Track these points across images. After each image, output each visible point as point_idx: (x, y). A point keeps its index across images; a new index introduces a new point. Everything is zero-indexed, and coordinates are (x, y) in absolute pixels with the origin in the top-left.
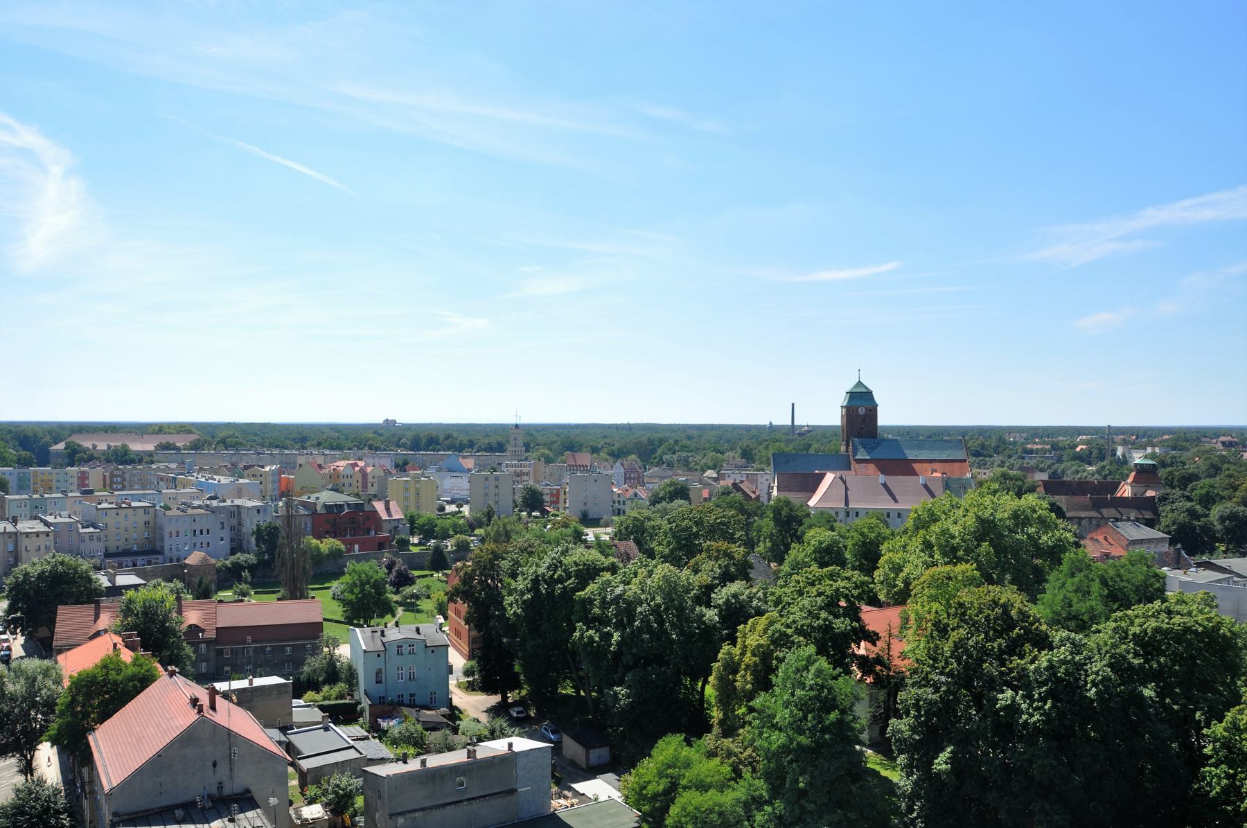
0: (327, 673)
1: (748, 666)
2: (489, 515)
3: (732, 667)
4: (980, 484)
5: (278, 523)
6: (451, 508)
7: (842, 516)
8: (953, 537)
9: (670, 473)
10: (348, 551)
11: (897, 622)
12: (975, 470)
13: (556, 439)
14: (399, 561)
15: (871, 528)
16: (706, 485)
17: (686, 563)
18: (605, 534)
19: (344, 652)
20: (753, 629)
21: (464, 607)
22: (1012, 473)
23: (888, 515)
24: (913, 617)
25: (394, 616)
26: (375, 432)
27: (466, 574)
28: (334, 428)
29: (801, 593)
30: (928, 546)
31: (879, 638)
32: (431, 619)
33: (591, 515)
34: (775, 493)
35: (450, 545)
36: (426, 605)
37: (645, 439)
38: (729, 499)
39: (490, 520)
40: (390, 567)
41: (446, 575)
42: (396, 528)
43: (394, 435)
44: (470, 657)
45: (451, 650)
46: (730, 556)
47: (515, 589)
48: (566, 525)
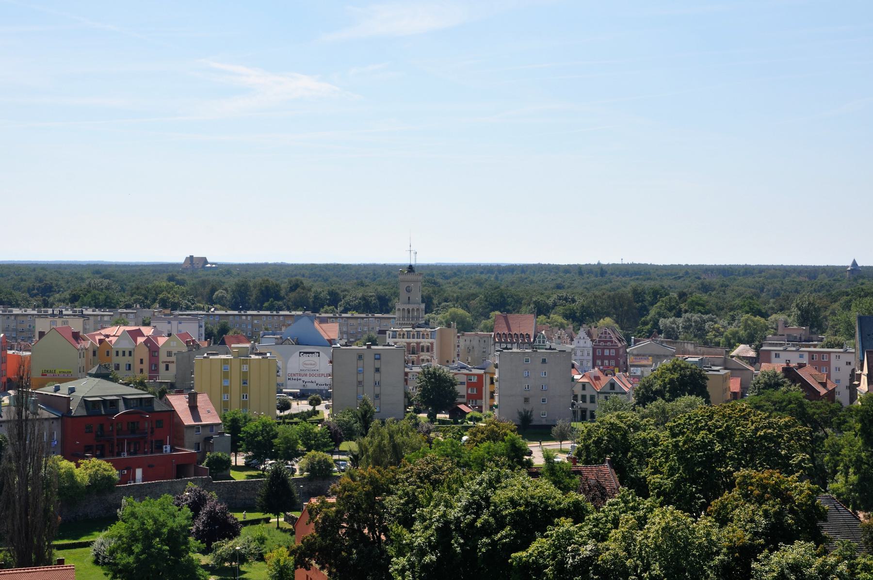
2: (365, 418)
6: (303, 406)
9: (672, 349)
10: (124, 479)
13: (475, 289)
16: (736, 371)
17: (704, 507)
18: (562, 451)
26: (171, 279)
27: (324, 520)
28: (100, 270)
33: (538, 419)
34: (864, 386)
35: (298, 467)
38: (778, 395)
39: (366, 427)
40: (196, 506)
41: (292, 520)
42: (208, 439)
43: (203, 283)
47: (410, 546)
48: (494, 436)
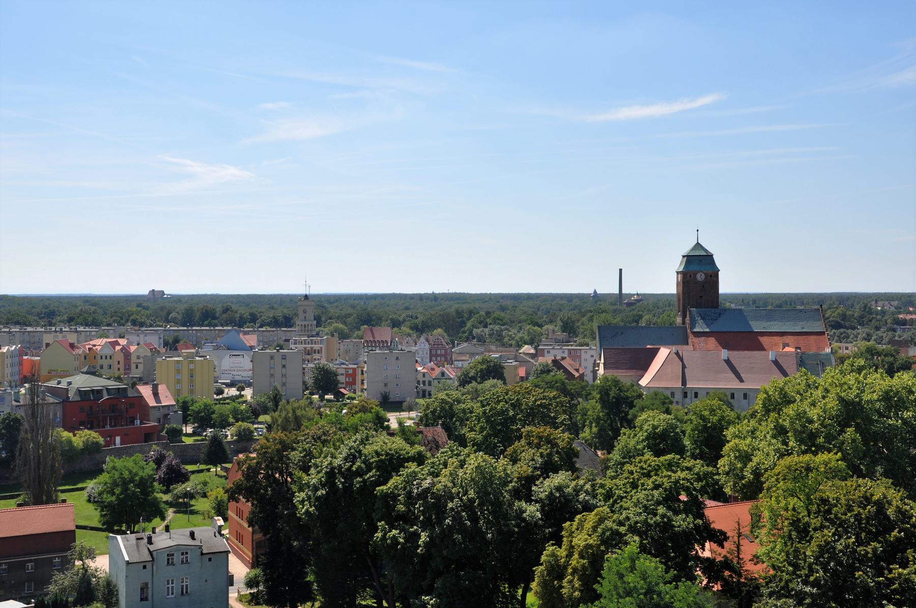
0: (79, 593)
1: (575, 570)
2: (276, 399)
3: (557, 571)
4: (842, 360)
5: (20, 414)
6: (233, 392)
7: (678, 397)
8: (811, 422)
10: (108, 444)
11: (746, 519)
12: (835, 345)
13: (350, 311)
14: (170, 455)
15: (712, 411)
16: (523, 362)
17: (502, 452)
18: (410, 418)
19: (101, 564)
20: (580, 527)
21: (247, 506)
22: (880, 347)
23: (733, 396)
24: (766, 514)
25: (163, 518)
26: (139, 306)
29: (634, 486)
30: (780, 432)
31: (726, 538)
32: (208, 521)
33: (392, 398)
34: (601, 371)
35: (230, 434)
36: (201, 505)
37: (452, 310)
38: (549, 378)
39: (277, 405)
40: (159, 461)
42: (166, 416)
43: (162, 308)
44: (254, 565)
45: (232, 558)
46: (551, 442)
